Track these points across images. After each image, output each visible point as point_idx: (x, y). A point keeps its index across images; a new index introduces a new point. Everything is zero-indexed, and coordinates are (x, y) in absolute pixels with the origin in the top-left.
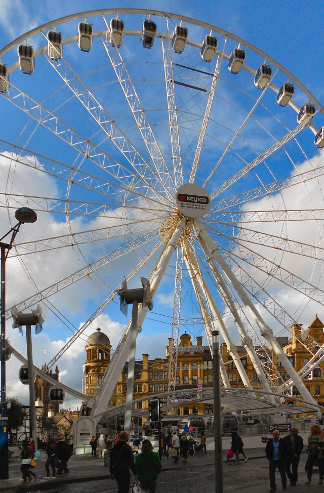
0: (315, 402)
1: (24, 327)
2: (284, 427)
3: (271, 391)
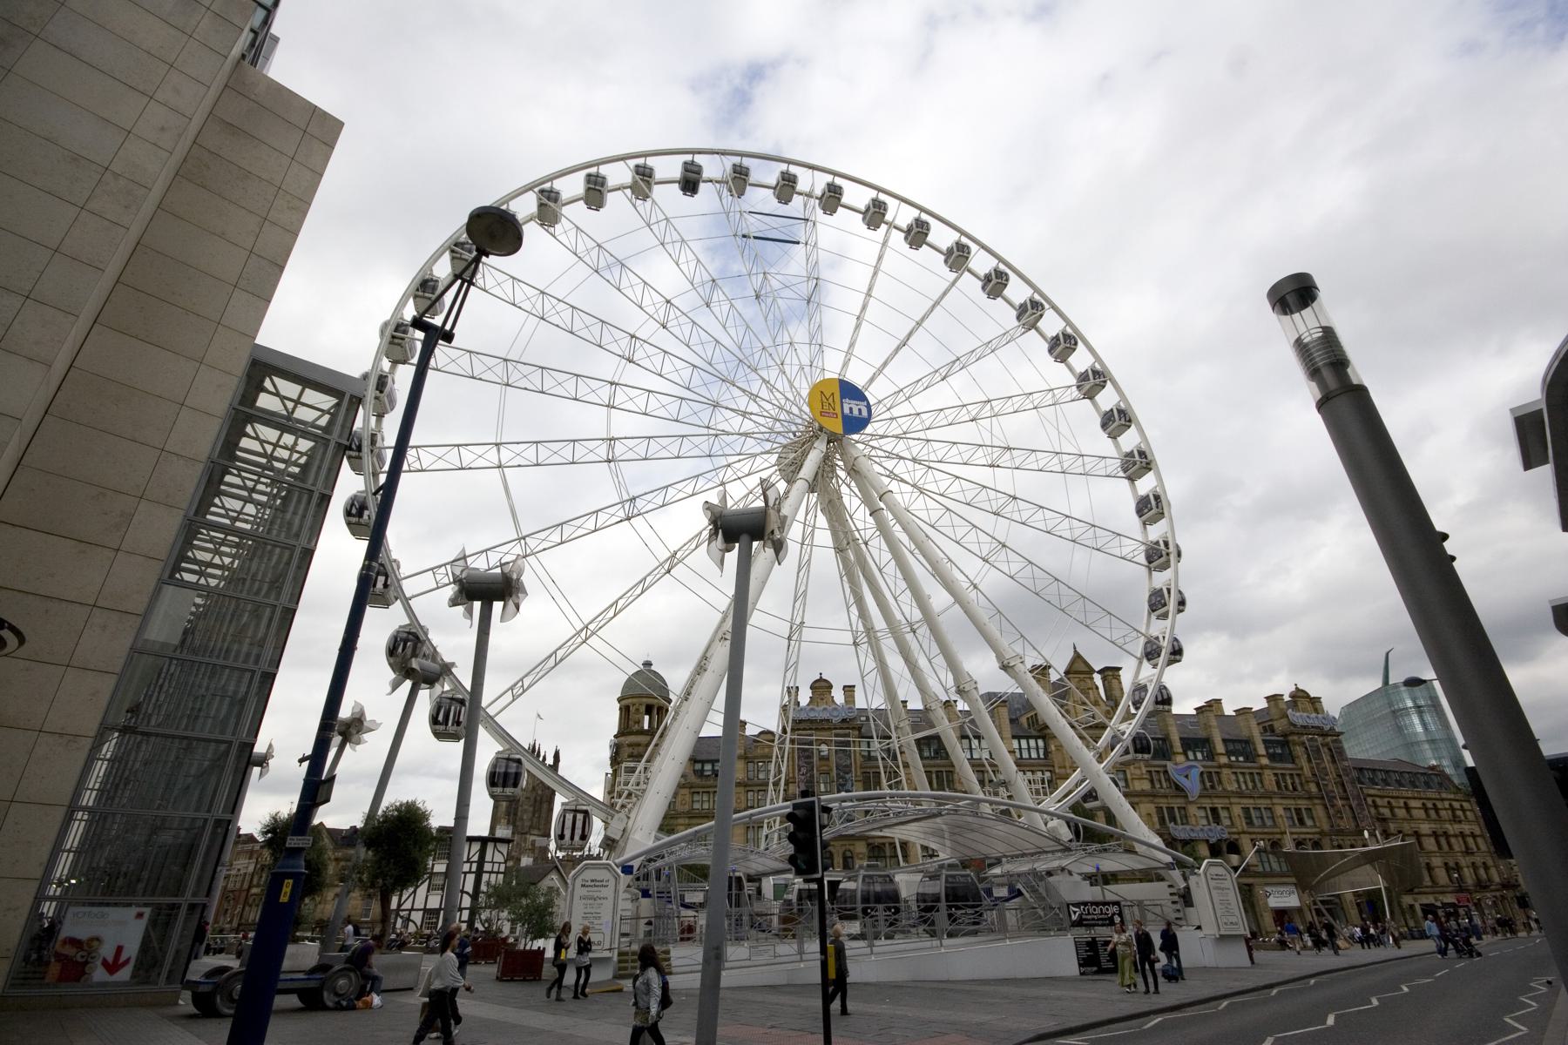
0: (1156, 840)
1: (477, 605)
2: (1104, 909)
3: (1032, 805)
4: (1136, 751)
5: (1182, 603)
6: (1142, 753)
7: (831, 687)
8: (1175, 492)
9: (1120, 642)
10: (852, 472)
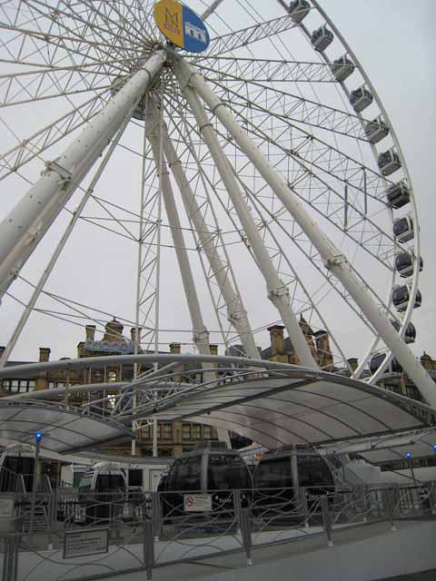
4: (394, 370)
5: (419, 299)
6: (398, 371)
8: (408, 156)
9: (382, 258)
10: (187, 90)
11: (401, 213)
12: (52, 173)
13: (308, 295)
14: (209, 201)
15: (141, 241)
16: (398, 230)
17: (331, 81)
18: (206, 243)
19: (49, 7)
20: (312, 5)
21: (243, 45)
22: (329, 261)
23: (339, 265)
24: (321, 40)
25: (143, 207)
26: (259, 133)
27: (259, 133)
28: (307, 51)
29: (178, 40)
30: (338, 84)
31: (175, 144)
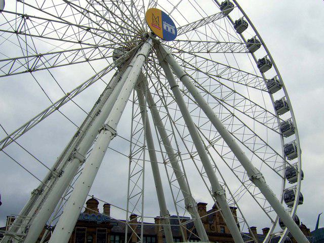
7: (98, 203)
8: (299, 124)
9: (276, 170)
11: (289, 140)
12: (107, 131)
13: (231, 195)
14: (173, 133)
15: (130, 157)
16: (287, 152)
17: (246, 52)
18: (173, 158)
19: (81, 8)
20: (235, 5)
21: (193, 29)
22: (252, 176)
23: (259, 179)
24: (240, 26)
25: (132, 136)
26: (201, 88)
27: (201, 88)
28: (253, 68)
29: (159, 33)
30: (250, 54)
31: (153, 95)
